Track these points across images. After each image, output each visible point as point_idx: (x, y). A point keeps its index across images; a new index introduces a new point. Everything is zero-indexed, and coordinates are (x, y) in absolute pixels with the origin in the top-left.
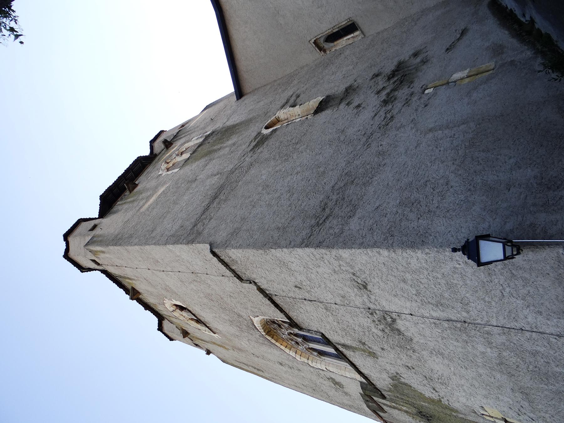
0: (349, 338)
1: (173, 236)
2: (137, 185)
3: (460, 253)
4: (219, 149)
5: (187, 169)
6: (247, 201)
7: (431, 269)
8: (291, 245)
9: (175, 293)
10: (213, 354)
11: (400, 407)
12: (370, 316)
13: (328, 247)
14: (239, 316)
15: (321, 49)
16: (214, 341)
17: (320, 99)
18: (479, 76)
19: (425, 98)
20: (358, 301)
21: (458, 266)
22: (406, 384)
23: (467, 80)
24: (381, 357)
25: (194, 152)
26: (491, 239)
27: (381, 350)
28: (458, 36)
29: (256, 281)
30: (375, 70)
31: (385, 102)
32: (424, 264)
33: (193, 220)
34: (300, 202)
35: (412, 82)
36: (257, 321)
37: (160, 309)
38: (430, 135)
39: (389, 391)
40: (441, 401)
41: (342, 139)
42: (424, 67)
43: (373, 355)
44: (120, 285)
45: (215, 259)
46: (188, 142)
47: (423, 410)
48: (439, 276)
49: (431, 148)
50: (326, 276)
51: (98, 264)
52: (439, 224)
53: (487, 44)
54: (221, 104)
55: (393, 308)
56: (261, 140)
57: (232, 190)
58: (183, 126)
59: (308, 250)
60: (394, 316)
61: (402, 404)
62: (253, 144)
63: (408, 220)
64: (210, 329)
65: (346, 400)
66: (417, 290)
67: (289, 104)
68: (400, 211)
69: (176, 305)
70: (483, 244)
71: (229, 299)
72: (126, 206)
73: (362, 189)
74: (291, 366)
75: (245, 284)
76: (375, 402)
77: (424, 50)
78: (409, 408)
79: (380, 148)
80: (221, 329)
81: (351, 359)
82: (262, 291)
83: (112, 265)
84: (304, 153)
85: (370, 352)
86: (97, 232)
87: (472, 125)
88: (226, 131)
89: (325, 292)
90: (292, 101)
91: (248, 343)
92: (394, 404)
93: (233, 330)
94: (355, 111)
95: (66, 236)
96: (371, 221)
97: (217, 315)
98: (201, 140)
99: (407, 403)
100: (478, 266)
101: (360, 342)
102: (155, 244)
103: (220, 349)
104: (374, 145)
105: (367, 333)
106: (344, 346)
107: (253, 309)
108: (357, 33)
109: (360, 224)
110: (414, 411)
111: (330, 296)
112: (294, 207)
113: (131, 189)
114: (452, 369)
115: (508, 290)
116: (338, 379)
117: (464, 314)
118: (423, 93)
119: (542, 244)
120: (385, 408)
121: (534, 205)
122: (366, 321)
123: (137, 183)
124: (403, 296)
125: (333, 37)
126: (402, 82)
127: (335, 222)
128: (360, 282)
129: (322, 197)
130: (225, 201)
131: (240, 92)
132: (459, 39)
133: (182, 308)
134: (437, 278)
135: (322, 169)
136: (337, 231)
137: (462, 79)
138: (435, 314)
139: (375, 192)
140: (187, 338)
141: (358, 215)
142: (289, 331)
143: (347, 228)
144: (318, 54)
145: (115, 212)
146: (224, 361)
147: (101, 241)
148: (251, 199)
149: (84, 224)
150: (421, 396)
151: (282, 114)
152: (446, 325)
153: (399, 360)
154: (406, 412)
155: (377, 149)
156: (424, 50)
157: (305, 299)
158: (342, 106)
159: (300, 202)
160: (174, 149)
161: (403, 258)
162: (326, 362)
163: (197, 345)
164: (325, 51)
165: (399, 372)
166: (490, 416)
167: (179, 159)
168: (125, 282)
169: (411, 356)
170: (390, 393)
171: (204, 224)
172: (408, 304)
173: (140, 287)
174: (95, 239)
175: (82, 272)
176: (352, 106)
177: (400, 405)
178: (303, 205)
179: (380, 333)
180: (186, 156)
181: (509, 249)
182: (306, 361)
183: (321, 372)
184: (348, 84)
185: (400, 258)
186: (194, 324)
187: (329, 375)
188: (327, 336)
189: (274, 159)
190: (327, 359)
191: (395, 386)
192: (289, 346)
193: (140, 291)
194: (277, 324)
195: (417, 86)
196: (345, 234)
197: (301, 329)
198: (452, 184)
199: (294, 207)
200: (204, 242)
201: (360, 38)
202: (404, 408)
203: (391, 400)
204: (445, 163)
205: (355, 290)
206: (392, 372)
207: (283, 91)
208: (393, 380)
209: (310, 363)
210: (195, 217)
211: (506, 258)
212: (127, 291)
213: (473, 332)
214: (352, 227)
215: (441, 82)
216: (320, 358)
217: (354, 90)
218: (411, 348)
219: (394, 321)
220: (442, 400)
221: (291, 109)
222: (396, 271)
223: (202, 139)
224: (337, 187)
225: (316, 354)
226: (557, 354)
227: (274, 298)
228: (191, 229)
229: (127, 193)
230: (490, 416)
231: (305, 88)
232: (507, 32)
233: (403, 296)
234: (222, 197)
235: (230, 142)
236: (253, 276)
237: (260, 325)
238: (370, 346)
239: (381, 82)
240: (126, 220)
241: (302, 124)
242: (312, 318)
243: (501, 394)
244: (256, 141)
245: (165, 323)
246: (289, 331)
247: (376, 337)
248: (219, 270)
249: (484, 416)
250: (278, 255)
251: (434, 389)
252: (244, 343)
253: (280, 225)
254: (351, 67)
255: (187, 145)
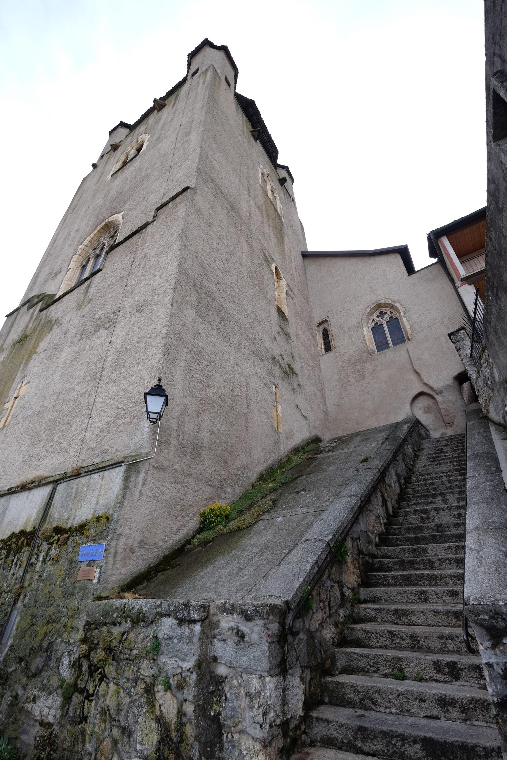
0: (95, 291)
1: (207, 157)
2: (256, 141)
3: (156, 382)
4: (269, 224)
5: (259, 191)
6: (224, 233)
7: (146, 362)
8: (182, 259)
9: (154, 146)
10: (93, 171)
11: (32, 322)
12: (113, 311)
13: (175, 288)
14: (125, 202)
15: (320, 324)
16: (105, 174)
17: (287, 315)
18: (276, 422)
19: (270, 385)
20: (127, 304)
21: (146, 381)
22: (51, 329)
23: (275, 413)
24: (77, 314)
25: (271, 202)
26: (164, 406)
27: (82, 314)
28: (304, 414)
29: (155, 222)
30: (296, 357)
31: (274, 359)
32: (151, 358)
33: (217, 181)
34: (215, 276)
35: (282, 379)
36: (118, 217)
37: (142, 128)
38: (244, 383)
39: (46, 315)
40: (36, 353)
41: (255, 322)
42: (290, 389)
43: (79, 307)
44: (169, 94)
45: (180, 190)
46: (280, 200)
47: (28, 339)
48: (140, 367)
49: (236, 381)
50: (152, 282)
51: (193, 75)
52: (180, 374)
53: (294, 430)
54: (301, 238)
55: (117, 329)
56: (268, 260)
57: (235, 224)
58: (293, 200)
59: (175, 271)
60: (111, 330)
61: (35, 324)
62: (267, 254)
63: (187, 353)
64: (116, 173)
65: (40, 280)
66: (130, 350)
67: (289, 291)
68: (194, 349)
69: (142, 146)
70: (162, 399)
71: (142, 196)
72: (241, 122)
73: (216, 326)
74: (75, 239)
75: (153, 212)
76: (37, 303)
77: (301, 392)
78: (30, 329)
79: (243, 347)
80: (115, 183)
81: (76, 290)
82: (146, 225)
83: (190, 89)
84: (251, 291)
85: (81, 306)
86: (224, 84)
87: (245, 411)
88: (281, 235)
89: (138, 278)
90: (290, 293)
91: (99, 205)
92: (35, 317)
93: (113, 193)
94: (273, 337)
95: (224, 49)
96: (191, 326)
97: (128, 182)
98: (279, 212)
99: (35, 329)
100: (145, 393)
101: (91, 300)
102: (203, 137)
103: (96, 178)
104: (247, 343)
105: (98, 306)
106: (89, 287)
107: (130, 215)
108: (324, 351)
109: (190, 317)
110: (28, 333)
111: (134, 283)
112: (212, 270)
113: (254, 133)
114: (62, 366)
115: (123, 412)
116: (60, 277)
117: (107, 381)
118: (274, 385)
119: (155, 439)
120: (31, 310)
121: (183, 439)
122: (109, 307)
123: (258, 141)
124: (127, 338)
125: (326, 334)
126: (284, 372)
127: (195, 299)
128: (142, 308)
129: (216, 295)
130: (228, 215)
131: (306, 255)
132: (302, 414)
133: (139, 150)
134: (138, 365)
135: (236, 300)
136: (188, 298)
137: (277, 411)
138: (109, 359)
139: (212, 335)
140: (110, 148)
141: (199, 320)
142: (106, 244)
143: (188, 307)
144: (317, 320)
145: (237, 110)
146: (84, 179)
147: (214, 84)
148: (225, 237)
149: (233, 74)
150: (40, 339)
151: (283, 282)
152: (99, 366)
153: (72, 327)
154: (27, 326)
155: (243, 344)
156: (301, 392)
157: (133, 261)
158: (277, 327)
159: (215, 276)
160: (277, 186)
161: (158, 343)
162: (75, 270)
163: (102, 156)
164: (318, 326)
165: (62, 325)
166: (21, 387)
167: (269, 188)
168: (172, 98)
169: (75, 337)
170: (44, 316)
171: (212, 189)
172: (119, 342)
173: (166, 112)
174: (217, 79)
175: (189, 55)
176: (276, 335)
177: (34, 322)
178: (212, 279)
179: (97, 316)
180: (270, 194)
181: (155, 416)
182: (78, 253)
183: (67, 264)
184: (292, 337)
185: (158, 341)
186: (123, 158)
187: (64, 270)
188: (99, 274)
189: (252, 266)
190: (79, 271)
191: (50, 321)
192: (93, 241)
193: (161, 113)
194: (114, 235)
195: (278, 382)
196: (184, 304)
197: (107, 253)
198: (208, 389)
199: (212, 270)
200: (197, 184)
201: (320, 352)
202: (30, 325)
203: (38, 316)
204: (223, 388)
205: (137, 303)
206: (63, 321)
207: (298, 289)
208: (56, 320)
209: (76, 256)
210: (220, 184)
211: (148, 413)
212: (164, 99)
213: (91, 385)
214: (188, 311)
215: (278, 397)
216: (80, 266)
217: (287, 339)
218: (82, 338)
219: (107, 328)
220: (36, 355)
221: (285, 291)
222: (149, 336)
223: (280, 213)
224: (221, 308)
225: (84, 263)
226: (69, 438)
227: (137, 235)
228: (210, 175)
229: (251, 129)
230: (21, 387)
231: (297, 306)
232: (298, 443)
233: (127, 338)
234: (232, 213)
235: (272, 235)
236: (160, 220)
237: (114, 219)
238: (87, 307)
239: (288, 359)
240: (229, 118)
241: (272, 295)
242: (116, 265)
243: (39, 397)
244: (268, 257)
245: (126, 131)
246: (106, 244)
247: (95, 312)
248: (170, 192)
249: (21, 383)
250: (175, 246)
251: (45, 350)
252: (99, 201)
253: (200, 255)
254: (303, 341)
255: (278, 198)
